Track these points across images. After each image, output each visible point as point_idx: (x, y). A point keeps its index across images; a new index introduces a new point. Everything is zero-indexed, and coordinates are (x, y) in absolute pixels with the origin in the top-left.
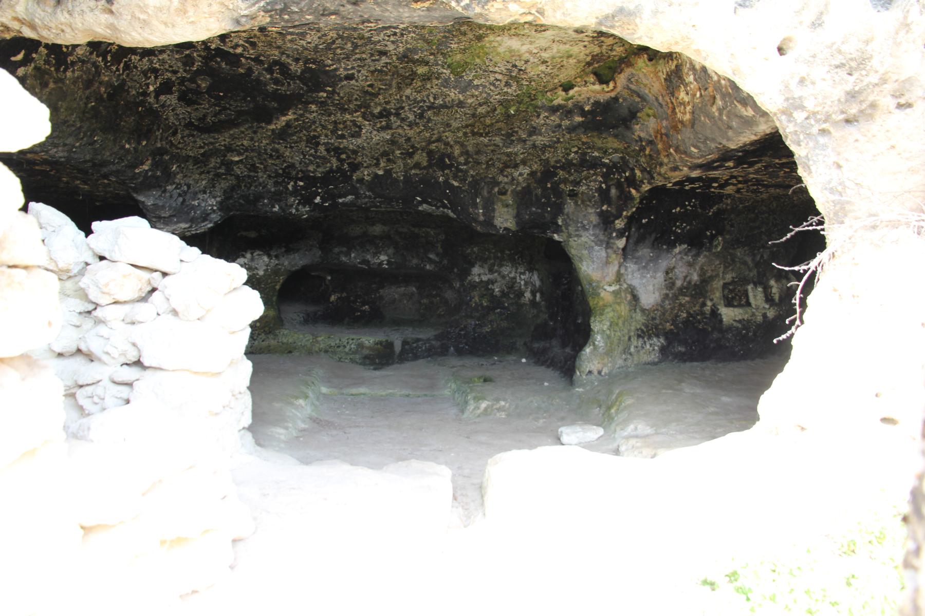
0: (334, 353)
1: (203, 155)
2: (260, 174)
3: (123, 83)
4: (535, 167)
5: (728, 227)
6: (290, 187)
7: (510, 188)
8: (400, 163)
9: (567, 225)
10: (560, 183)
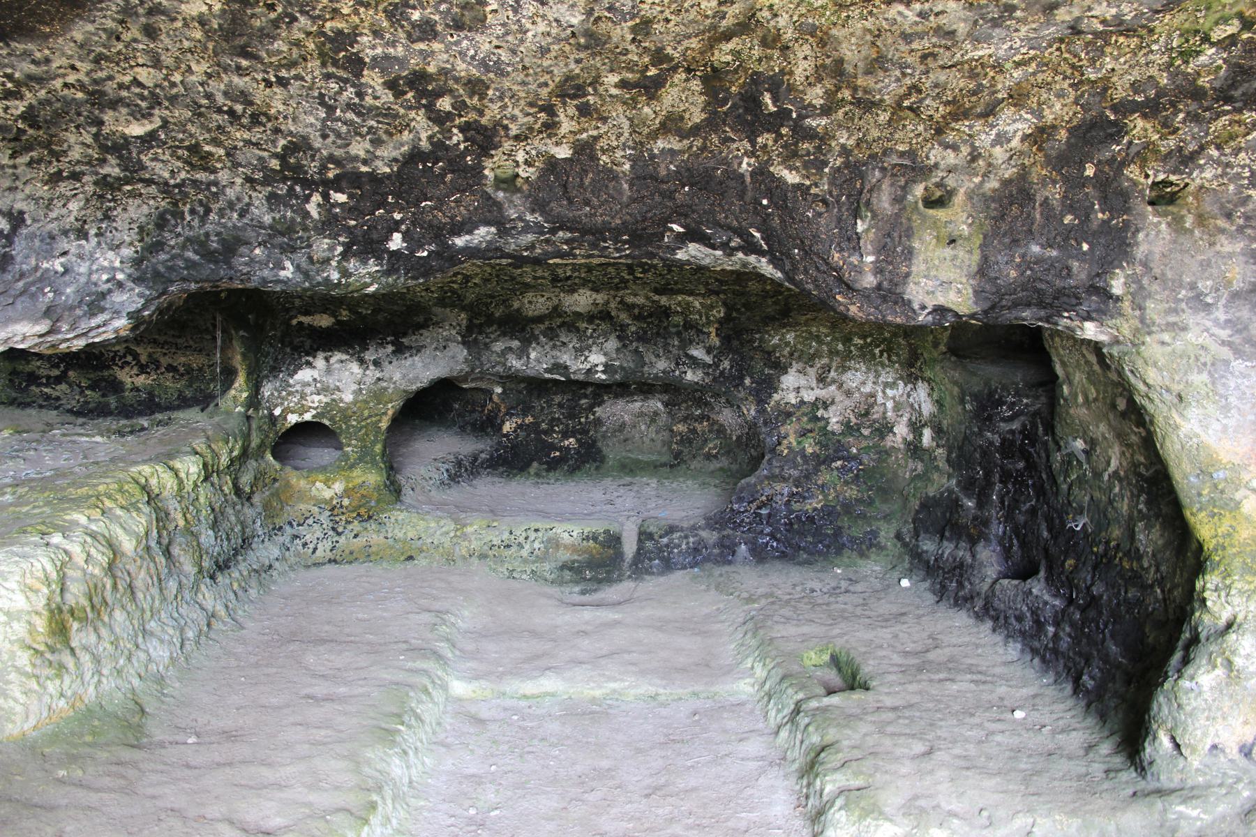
0: (499, 560)
1: (29, 116)
2: (223, 176)
6: (312, 208)
7: (963, 185)
8: (619, 116)
9: (1139, 296)
10: (1124, 164)
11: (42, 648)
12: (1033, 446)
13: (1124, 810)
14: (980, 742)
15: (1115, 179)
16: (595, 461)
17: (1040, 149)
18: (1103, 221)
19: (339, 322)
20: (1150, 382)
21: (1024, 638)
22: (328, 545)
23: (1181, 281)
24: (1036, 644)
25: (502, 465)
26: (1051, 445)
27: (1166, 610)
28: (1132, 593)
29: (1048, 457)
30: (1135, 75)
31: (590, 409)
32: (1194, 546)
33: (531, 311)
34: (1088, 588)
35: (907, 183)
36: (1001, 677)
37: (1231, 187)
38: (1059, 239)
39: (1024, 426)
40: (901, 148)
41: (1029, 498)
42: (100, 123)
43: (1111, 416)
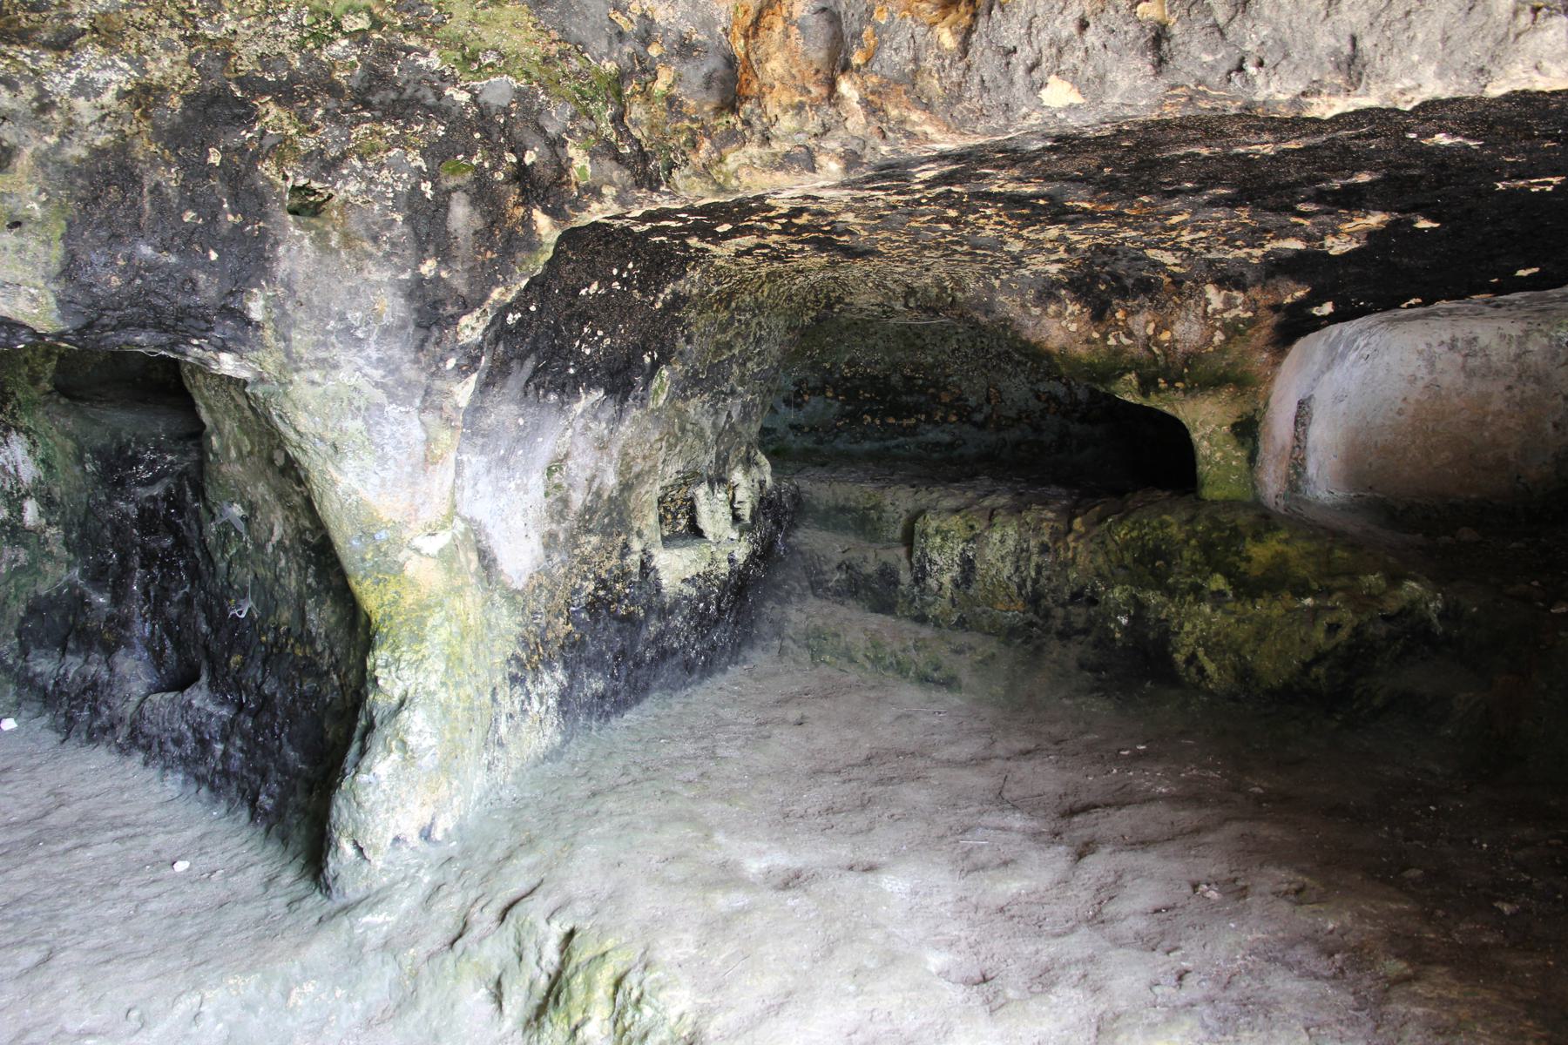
4: (164, 67)
5: (681, 343)
10: (257, 157)
12: (181, 516)
13: (308, 943)
14: (128, 918)
15: (247, 174)
17: (145, 115)
18: (235, 226)
20: (302, 429)
21: (187, 765)
23: (329, 309)
24: (202, 770)
26: (203, 513)
27: (344, 698)
28: (308, 684)
29: (200, 529)
30: (261, 46)
32: (363, 620)
34: (259, 687)
36: (156, 824)
37: (376, 207)
38: (177, 241)
39: (168, 490)
41: (181, 584)
43: (269, 473)
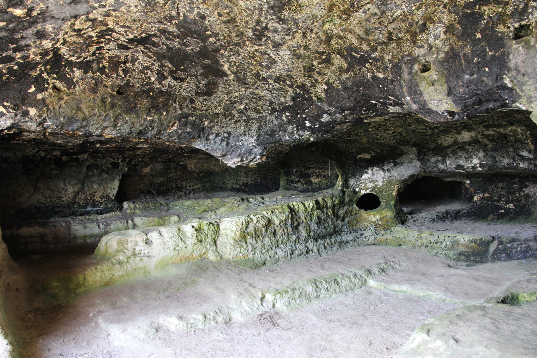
3: (128, 82)
4: (446, 18)
11: (237, 240)
16: (525, 215)
17: (453, 35)
18: (492, 55)
19: (372, 156)
22: (373, 238)
25: (473, 216)
31: (520, 189)
33: (446, 144)
35: (411, 66)
40: (406, 53)
42: (235, 108)
